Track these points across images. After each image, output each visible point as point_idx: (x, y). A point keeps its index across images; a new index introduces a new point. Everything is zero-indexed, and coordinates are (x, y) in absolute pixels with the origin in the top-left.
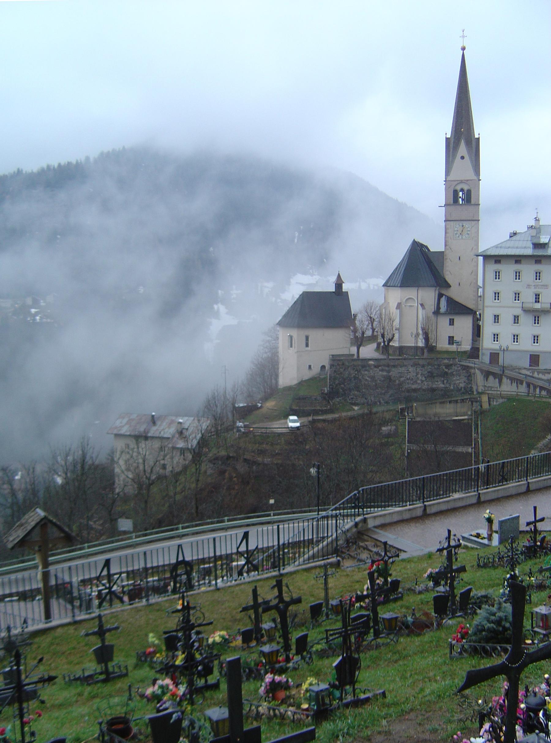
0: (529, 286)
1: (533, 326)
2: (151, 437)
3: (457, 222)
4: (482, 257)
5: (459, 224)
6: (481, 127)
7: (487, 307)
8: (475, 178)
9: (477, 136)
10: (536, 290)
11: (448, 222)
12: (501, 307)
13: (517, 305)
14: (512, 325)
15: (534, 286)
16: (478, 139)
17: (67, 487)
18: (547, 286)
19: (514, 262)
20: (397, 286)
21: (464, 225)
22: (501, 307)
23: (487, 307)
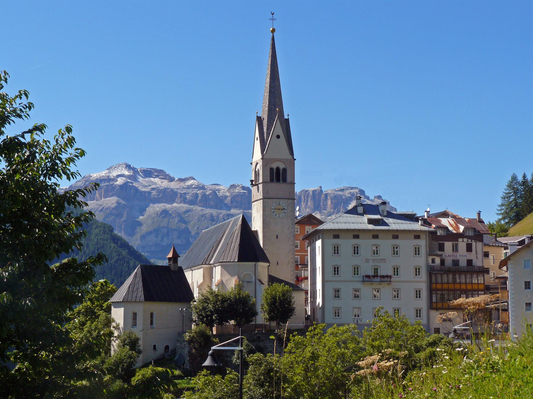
0: (367, 261)
1: (373, 299)
2: (457, 245)
3: (274, 200)
4: (362, 207)
5: (276, 203)
6: (288, 110)
7: (327, 281)
8: (290, 157)
9: (286, 117)
10: (374, 264)
11: (266, 200)
12: (341, 281)
13: (357, 279)
14: (353, 299)
15: (373, 260)
16: (288, 120)
17: (78, 288)
18: (384, 260)
19: (352, 236)
20: (140, 302)
21: (281, 203)
22: (341, 281)
23: (327, 281)
